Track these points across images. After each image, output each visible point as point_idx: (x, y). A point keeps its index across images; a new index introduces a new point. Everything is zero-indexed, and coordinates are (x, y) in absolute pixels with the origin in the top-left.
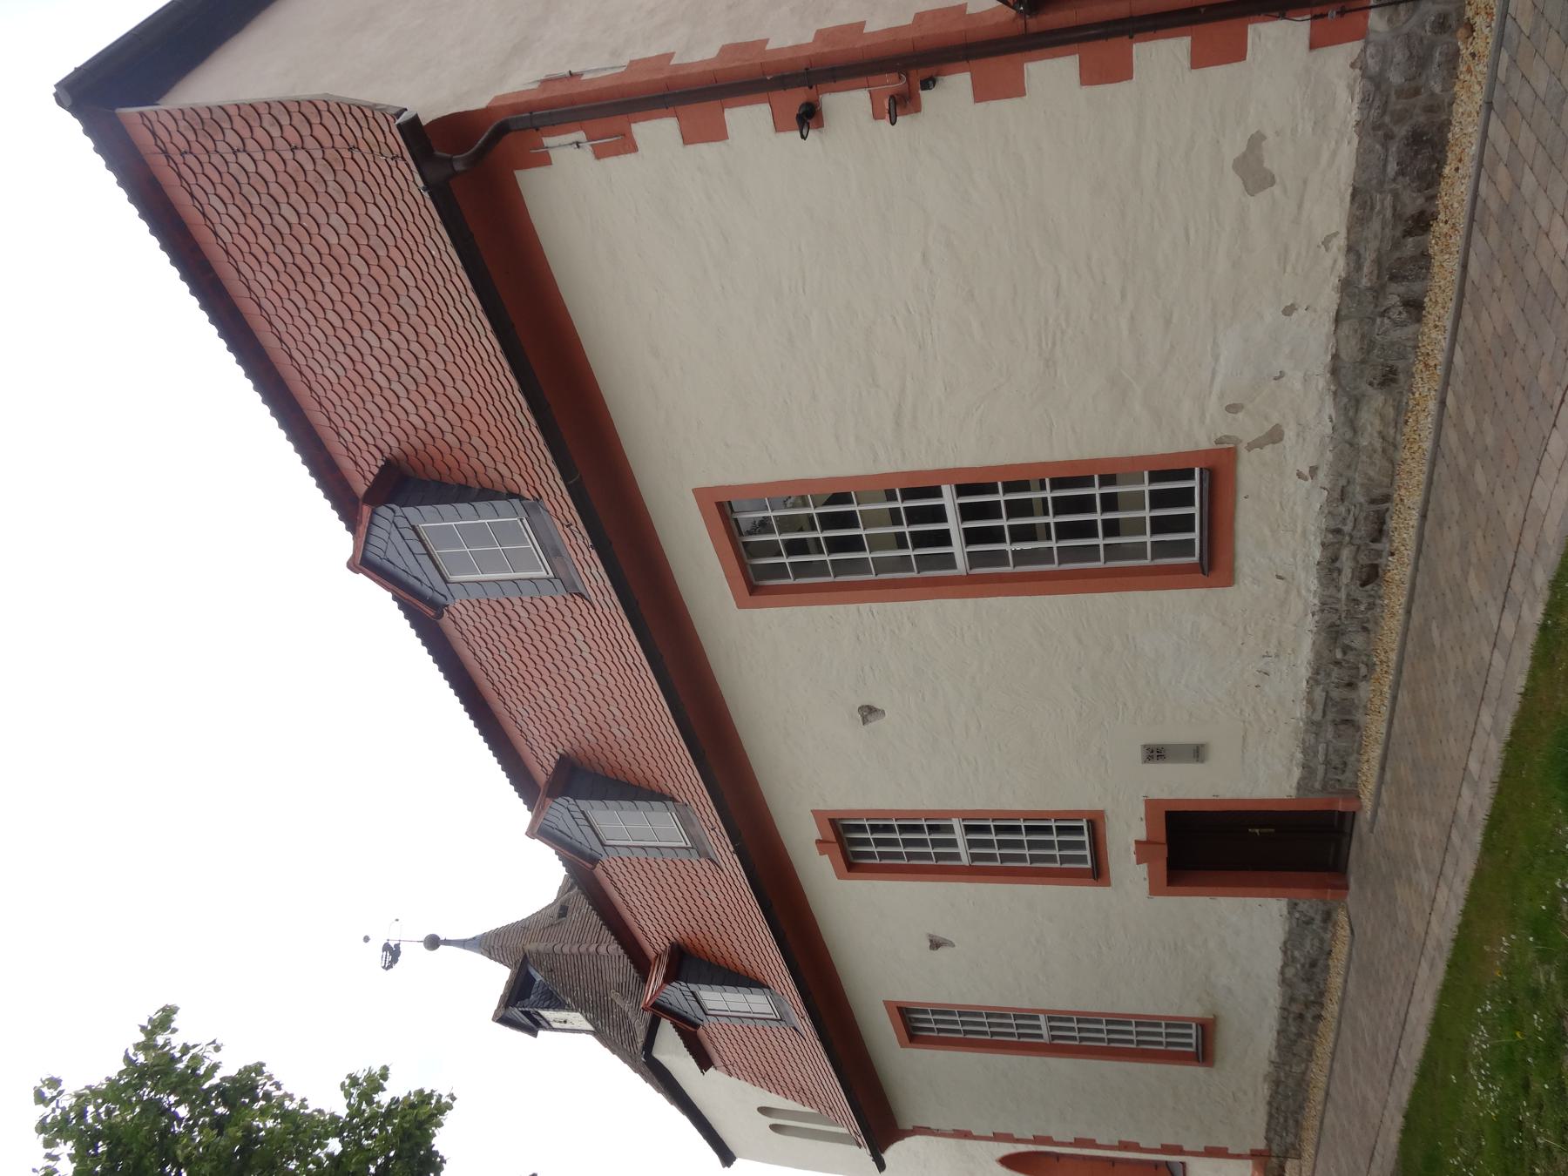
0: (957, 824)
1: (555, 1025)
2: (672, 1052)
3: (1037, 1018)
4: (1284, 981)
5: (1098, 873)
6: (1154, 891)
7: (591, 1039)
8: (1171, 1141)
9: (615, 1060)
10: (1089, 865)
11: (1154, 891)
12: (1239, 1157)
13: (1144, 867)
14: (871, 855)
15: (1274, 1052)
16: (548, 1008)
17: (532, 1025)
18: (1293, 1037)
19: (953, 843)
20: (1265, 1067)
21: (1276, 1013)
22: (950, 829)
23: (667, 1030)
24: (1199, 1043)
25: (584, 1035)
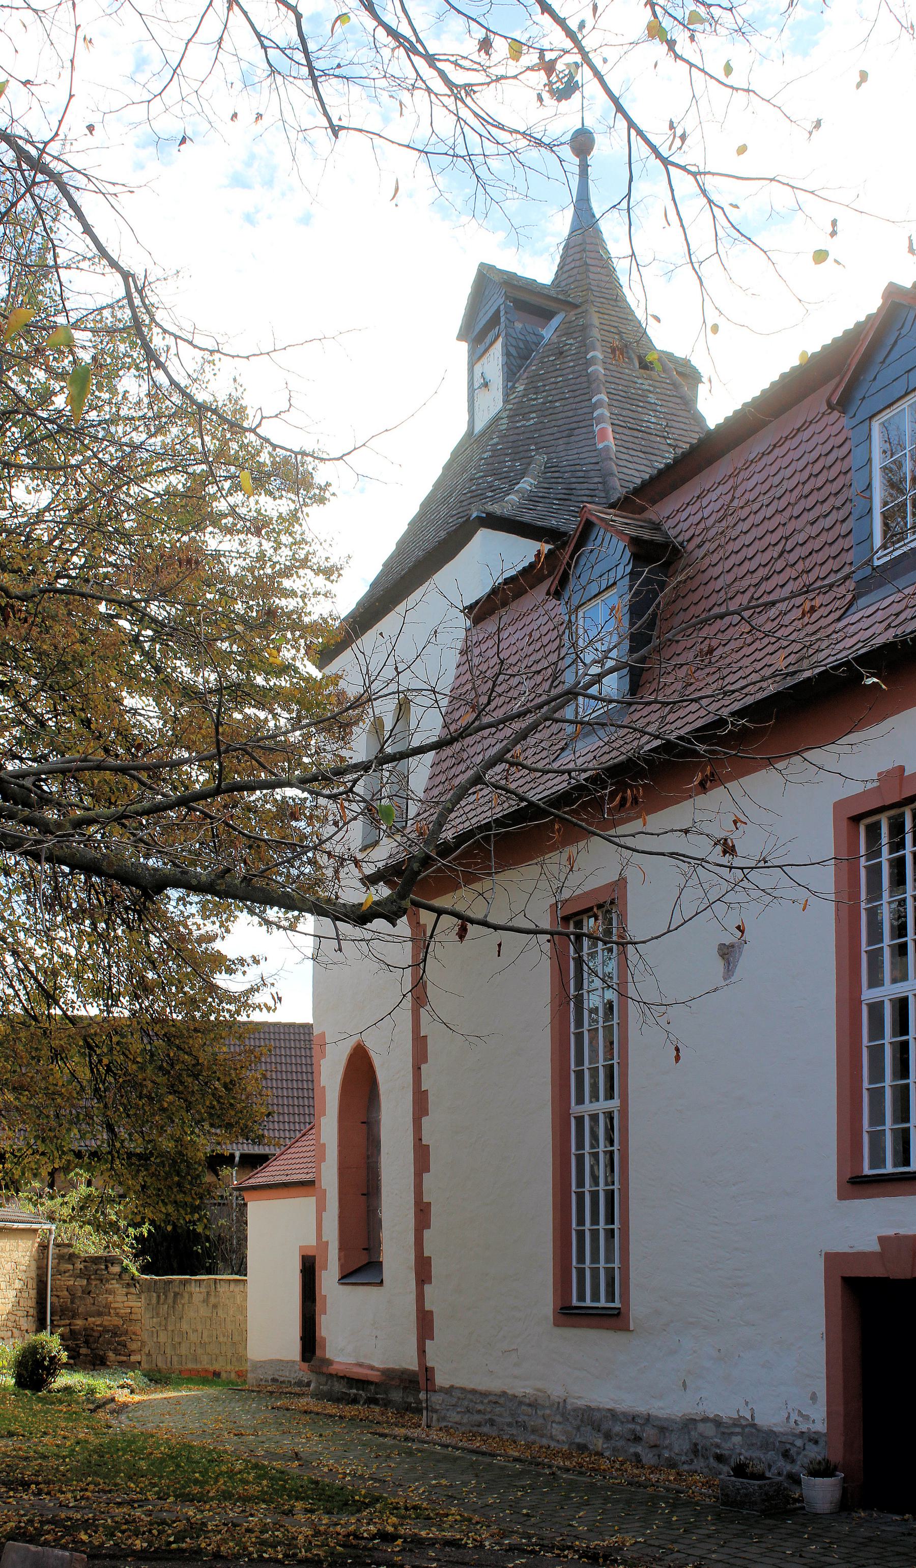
0: (614, 1104)
1: (478, 369)
2: (492, 557)
3: (610, 1096)
4: (689, 1423)
5: (857, 1184)
6: (832, 1260)
7: (463, 429)
8: (436, 1270)
9: (435, 472)
10: (867, 1171)
11: (832, 1260)
12: (422, 1352)
13: (877, 1248)
14: (874, 853)
15: (581, 1403)
16: (507, 354)
17: (478, 331)
18: (605, 1427)
19: (595, 1097)
20: (556, 1392)
21: (642, 1408)
22: (610, 1096)
23: (521, 552)
24: (590, 1303)
25: (466, 417)
